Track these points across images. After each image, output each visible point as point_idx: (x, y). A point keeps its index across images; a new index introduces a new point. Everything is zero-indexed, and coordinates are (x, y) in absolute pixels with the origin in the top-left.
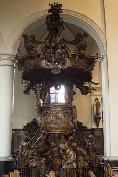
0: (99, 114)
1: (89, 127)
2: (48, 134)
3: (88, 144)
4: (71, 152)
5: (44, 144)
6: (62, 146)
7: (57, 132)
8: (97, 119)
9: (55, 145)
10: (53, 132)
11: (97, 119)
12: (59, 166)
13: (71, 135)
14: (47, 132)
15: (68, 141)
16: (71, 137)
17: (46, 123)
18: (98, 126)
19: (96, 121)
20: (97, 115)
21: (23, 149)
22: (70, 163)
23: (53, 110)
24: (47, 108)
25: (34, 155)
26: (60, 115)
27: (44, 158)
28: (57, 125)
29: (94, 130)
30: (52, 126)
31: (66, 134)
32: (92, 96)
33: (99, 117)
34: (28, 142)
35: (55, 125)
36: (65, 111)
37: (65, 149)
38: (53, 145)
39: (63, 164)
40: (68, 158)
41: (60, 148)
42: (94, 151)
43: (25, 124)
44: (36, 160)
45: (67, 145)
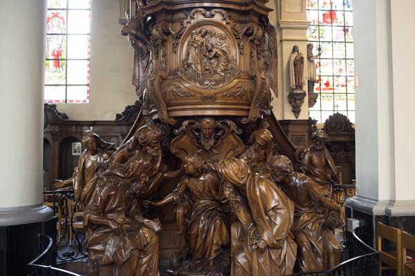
0: (302, 84)
2: (173, 121)
3: (311, 159)
4: (276, 197)
5: (154, 160)
6: (233, 169)
9: (199, 164)
10: (190, 113)
12: (217, 250)
15: (252, 148)
17: (163, 74)
18: (298, 115)
19: (295, 102)
20: (296, 89)
21: (87, 178)
27: (152, 222)
29: (289, 122)
30: (187, 85)
31: (244, 121)
32: (284, 42)
34: (103, 153)
35: (201, 83)
36: (242, 29)
37: (245, 185)
38: (191, 163)
39: (234, 243)
40: (259, 222)
41: (220, 181)
42: (328, 180)
44: (116, 233)
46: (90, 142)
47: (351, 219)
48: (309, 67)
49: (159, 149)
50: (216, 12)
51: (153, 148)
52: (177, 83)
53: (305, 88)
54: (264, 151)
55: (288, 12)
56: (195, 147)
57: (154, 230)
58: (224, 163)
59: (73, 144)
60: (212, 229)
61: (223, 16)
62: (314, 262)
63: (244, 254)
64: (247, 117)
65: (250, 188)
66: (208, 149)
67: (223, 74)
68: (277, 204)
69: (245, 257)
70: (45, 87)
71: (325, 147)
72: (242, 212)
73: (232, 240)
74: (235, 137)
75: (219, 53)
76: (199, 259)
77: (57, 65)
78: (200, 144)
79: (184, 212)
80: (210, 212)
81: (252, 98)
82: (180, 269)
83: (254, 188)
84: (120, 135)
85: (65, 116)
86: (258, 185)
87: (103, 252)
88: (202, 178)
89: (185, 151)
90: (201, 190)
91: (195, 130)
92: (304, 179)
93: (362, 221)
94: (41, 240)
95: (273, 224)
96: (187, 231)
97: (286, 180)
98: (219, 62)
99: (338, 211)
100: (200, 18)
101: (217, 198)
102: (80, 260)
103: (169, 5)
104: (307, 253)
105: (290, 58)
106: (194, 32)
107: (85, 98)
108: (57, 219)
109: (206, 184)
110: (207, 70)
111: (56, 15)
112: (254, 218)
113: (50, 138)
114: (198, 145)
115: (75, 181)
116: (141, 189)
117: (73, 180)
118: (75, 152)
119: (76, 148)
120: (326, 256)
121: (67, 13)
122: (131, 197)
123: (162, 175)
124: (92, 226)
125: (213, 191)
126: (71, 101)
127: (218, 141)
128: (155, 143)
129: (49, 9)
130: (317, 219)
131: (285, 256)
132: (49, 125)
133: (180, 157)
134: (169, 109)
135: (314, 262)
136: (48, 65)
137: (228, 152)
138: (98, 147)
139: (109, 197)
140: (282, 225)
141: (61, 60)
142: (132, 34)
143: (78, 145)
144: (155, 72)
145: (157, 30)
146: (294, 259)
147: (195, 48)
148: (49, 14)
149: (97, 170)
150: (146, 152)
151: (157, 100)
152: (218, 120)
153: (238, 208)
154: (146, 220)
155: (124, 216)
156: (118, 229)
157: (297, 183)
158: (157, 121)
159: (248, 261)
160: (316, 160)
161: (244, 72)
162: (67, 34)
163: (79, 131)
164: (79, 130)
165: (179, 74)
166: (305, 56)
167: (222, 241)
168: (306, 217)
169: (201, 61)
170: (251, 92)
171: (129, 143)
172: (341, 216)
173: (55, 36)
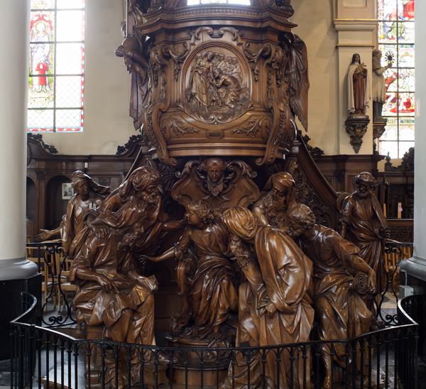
0: (364, 106)
1: (329, 150)
2: (174, 162)
3: (353, 209)
4: (289, 252)
5: (151, 207)
6: (237, 220)
7: (218, 152)
8: (357, 125)
9: (205, 213)
10: (196, 153)
11: (357, 125)
12: (223, 316)
13: (281, 166)
14: (169, 150)
15: (269, 195)
16: (286, 178)
17: (162, 106)
18: (359, 148)
20: (356, 112)
21: (77, 228)
22: (281, 311)
23: (193, 43)
24: (169, 32)
26: (234, 68)
27: (147, 279)
28: (217, 114)
29: (345, 158)
30: (190, 120)
31: (259, 162)
32: (340, 49)
33: (364, 117)
34: (96, 197)
35: (206, 117)
36: (257, 50)
37: (254, 238)
38: (195, 212)
39: (242, 307)
41: (227, 235)
42: (376, 236)
43: (124, 141)
44: (107, 290)
45: (264, 214)
46: (80, 185)
47: (403, 287)
48: (374, 84)
49: (156, 195)
50: (225, 31)
51: (149, 193)
52: (179, 118)
53: (369, 112)
54: (283, 198)
55: (346, 8)
56: (201, 193)
57: (148, 289)
58: (229, 212)
59: (64, 184)
61: (234, 35)
62: (336, 332)
63: (251, 319)
64: (263, 157)
65: (259, 242)
66: (215, 195)
67: (233, 106)
68: (289, 261)
69: (252, 322)
70: (28, 111)
73: (240, 303)
74: (247, 181)
75: (229, 80)
76: (203, 326)
77: (43, 83)
78: (206, 189)
79: (185, 270)
80: (216, 270)
81: (268, 135)
82: (181, 336)
83: (263, 242)
84: (121, 173)
85: (53, 149)
87: (90, 311)
88: (208, 230)
89: (189, 197)
91: (200, 173)
92: (328, 233)
93: (417, 289)
94: (25, 300)
96: (190, 291)
97: (306, 233)
98: (228, 91)
99: (367, 273)
100: (206, 38)
101: (225, 254)
102: (68, 326)
103: (170, 24)
104: (328, 321)
105: (348, 71)
106: (200, 55)
107: (78, 124)
108: (41, 278)
109: (213, 237)
110: (214, 101)
111: (41, 18)
112: (264, 278)
113: (34, 177)
114: (205, 191)
115: (63, 231)
116: (135, 241)
117: (61, 230)
118: (65, 195)
119: (67, 191)
120: (352, 326)
121: (55, 15)
122: (125, 250)
123: (162, 226)
124: (78, 280)
125: (221, 246)
126: (61, 129)
127: (228, 185)
128: (151, 188)
129: (32, 10)
131: (299, 323)
132: (33, 161)
133: (183, 204)
134: (169, 147)
136: (31, 83)
138: (89, 191)
139: (98, 250)
140: (295, 287)
141: (48, 76)
142: (128, 56)
143: (69, 185)
144: (153, 103)
145: (156, 54)
146: (310, 327)
147: (200, 75)
148: (32, 16)
149: (86, 219)
150: (141, 198)
151: (156, 138)
152: (227, 161)
154: (141, 277)
155: (114, 271)
156: (108, 285)
157: (319, 238)
158: (157, 161)
159: (255, 326)
160: (359, 210)
161: (259, 103)
162: (55, 42)
163: (70, 168)
164: (70, 166)
165: (181, 106)
166: (369, 68)
168: (330, 279)
169: (207, 92)
170: (266, 127)
171: (122, 188)
172: (371, 279)
173: (40, 45)
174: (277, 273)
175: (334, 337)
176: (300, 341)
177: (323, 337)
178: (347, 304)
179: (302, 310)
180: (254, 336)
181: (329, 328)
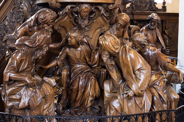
12: (91, 101)
15: (114, 27)
22: (138, 95)
25: (23, 71)
37: (118, 53)
38: (75, 37)
39: (107, 95)
44: (28, 86)
51: (49, 25)
54: (123, 29)
56: (73, 26)
60: (90, 85)
63: (117, 100)
64: (113, 4)
71: (156, 28)
72: (115, 72)
78: (77, 23)
79: (67, 74)
86: (129, 53)
88: (79, 49)
89: (65, 28)
90: (78, 58)
95: (138, 79)
97: (142, 50)
101: (90, 63)
104: (157, 101)
128: (51, 22)
130: (162, 79)
135: (161, 107)
137: (96, 29)
139: (21, 61)
140: (144, 81)
146: (150, 104)
153: (112, 69)
167: (96, 93)
174: (134, 74)
175: (160, 109)
176: (145, 112)
177: (154, 109)
178: (166, 91)
179: (146, 95)
180: (119, 111)
181: (157, 105)
